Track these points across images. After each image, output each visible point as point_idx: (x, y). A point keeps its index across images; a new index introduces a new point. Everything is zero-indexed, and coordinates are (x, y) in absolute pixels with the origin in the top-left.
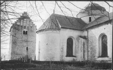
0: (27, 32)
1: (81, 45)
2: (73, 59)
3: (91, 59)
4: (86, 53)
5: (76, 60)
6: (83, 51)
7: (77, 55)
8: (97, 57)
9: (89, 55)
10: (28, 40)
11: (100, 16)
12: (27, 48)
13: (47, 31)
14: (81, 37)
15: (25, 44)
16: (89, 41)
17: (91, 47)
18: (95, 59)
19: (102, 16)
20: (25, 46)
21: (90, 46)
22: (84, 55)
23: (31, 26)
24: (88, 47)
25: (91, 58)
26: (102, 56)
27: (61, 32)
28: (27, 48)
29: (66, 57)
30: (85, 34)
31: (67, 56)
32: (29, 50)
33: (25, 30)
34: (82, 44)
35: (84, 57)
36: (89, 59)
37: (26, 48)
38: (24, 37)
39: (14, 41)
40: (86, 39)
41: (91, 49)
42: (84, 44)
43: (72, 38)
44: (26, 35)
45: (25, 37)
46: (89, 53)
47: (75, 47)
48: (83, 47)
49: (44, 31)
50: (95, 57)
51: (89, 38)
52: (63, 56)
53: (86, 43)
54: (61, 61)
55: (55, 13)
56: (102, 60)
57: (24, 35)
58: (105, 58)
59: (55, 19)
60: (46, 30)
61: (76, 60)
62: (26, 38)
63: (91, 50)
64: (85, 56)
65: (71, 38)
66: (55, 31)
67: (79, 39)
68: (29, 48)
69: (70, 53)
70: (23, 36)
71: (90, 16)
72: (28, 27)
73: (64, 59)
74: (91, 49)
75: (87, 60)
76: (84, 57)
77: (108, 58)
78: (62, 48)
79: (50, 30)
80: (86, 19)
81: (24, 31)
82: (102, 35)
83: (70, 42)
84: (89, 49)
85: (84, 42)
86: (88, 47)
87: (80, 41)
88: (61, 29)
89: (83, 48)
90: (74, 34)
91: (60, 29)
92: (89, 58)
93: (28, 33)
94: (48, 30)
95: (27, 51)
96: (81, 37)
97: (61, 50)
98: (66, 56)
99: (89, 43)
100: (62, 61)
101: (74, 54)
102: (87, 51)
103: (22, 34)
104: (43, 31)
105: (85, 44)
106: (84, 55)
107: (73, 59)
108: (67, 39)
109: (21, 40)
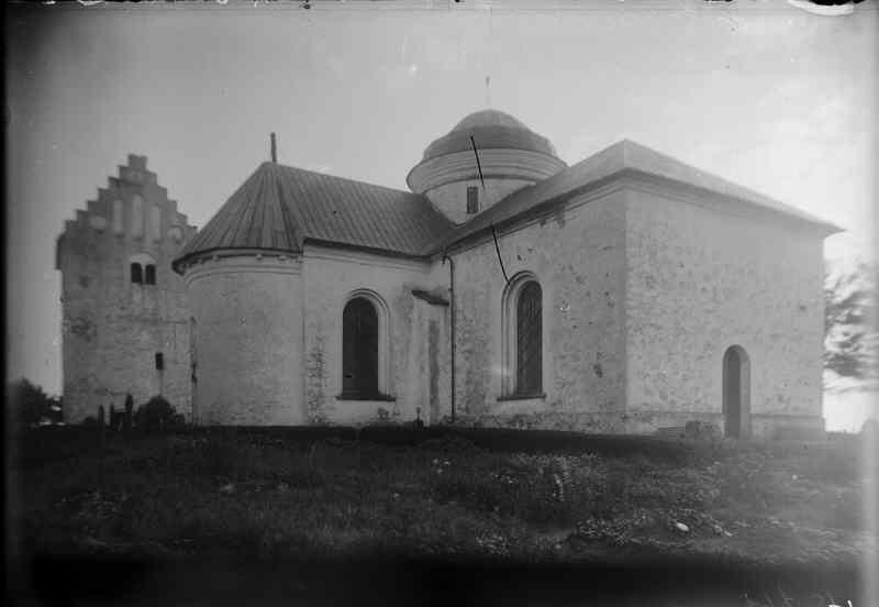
0: (151, 269)
1: (418, 339)
2: (381, 411)
3: (467, 409)
4: (444, 380)
5: (394, 414)
6: (427, 369)
7: (399, 389)
8: (494, 399)
9: (457, 389)
10: (163, 314)
11: (523, 183)
12: (159, 357)
13: (230, 261)
14: (419, 293)
15: (145, 337)
16: (459, 316)
17: (468, 346)
18: (487, 411)
19: (533, 183)
20: (149, 349)
21: (464, 341)
22: (434, 389)
23: (174, 237)
24: (453, 346)
25: (468, 402)
26: (519, 394)
27: (306, 268)
28: (159, 357)
29: (340, 404)
30: (436, 277)
31: (345, 396)
32: (168, 365)
33: (144, 260)
34: (427, 325)
35: (434, 400)
36: (457, 412)
37: (154, 359)
38: (137, 298)
39: (79, 323)
40: (445, 304)
41: (467, 354)
42: (433, 329)
43: (374, 301)
44: (151, 286)
45: (140, 296)
46: (461, 377)
47: (391, 350)
48: (427, 345)
49: (211, 258)
50: (484, 397)
51: (459, 300)
52: (321, 395)
53: (445, 324)
54: (307, 424)
55: (281, 161)
56: (517, 412)
57: (135, 285)
58: (528, 402)
59: (458, 238)
60: (220, 257)
61: (394, 414)
62: (150, 306)
63: (468, 365)
64: (440, 395)
65: (361, 299)
66: (275, 262)
67: (411, 307)
68: (167, 357)
69: (361, 376)
70: (131, 295)
71: (472, 183)
72: (156, 242)
73: (327, 412)
74: (467, 359)
75: (449, 414)
76: (434, 400)
77: (542, 404)
78: (318, 357)
79: (245, 251)
80: (452, 204)
81: (136, 267)
82: (523, 282)
83: (360, 319)
84: (459, 360)
85: (436, 319)
86: (453, 346)
87: (415, 315)
88: (307, 248)
89: (426, 356)
90: (385, 280)
91: (302, 252)
92: (457, 402)
93: (159, 277)
94: (230, 256)
95: (162, 375)
96: (419, 293)
97: (312, 364)
98: (338, 398)
99: (457, 326)
100: (316, 421)
101: (383, 385)
102: (449, 368)
103: (122, 278)
104: (205, 260)
105: (442, 332)
106: (434, 389)
107: (381, 411)
108: (345, 303)
109: (121, 317)
